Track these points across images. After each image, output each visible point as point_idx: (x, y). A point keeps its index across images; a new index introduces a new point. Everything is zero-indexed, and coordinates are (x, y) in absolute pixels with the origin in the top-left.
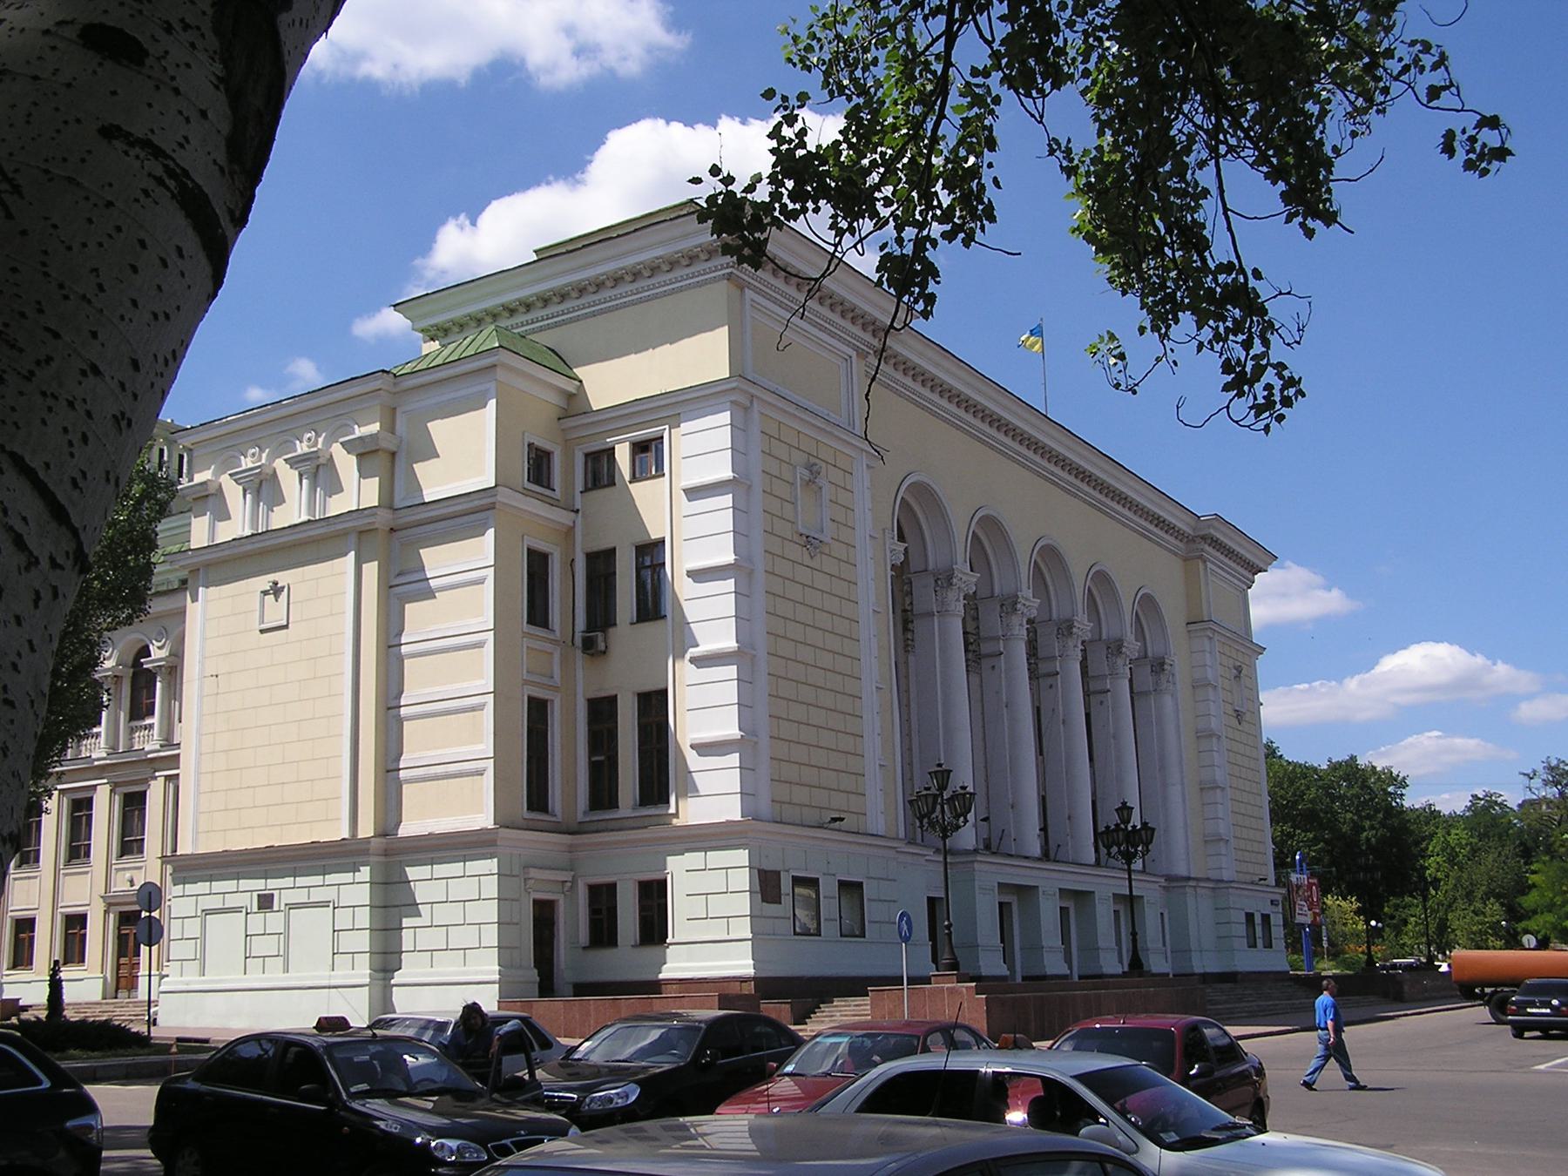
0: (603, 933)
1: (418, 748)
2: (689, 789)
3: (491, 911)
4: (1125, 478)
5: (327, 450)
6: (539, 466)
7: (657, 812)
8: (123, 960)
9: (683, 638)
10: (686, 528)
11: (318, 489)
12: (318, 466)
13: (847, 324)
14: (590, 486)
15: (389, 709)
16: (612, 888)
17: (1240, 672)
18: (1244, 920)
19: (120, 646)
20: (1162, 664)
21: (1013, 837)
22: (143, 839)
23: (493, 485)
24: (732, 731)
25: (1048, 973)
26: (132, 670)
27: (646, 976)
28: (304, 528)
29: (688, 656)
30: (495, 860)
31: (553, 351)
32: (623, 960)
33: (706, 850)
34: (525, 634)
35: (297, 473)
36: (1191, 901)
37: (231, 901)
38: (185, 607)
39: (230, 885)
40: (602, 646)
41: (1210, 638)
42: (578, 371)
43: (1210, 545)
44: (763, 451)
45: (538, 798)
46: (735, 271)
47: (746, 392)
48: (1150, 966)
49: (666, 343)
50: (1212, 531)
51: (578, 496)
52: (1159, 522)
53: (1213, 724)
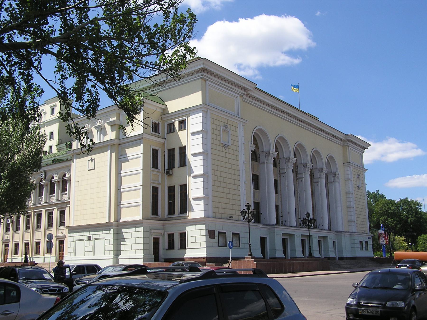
0: (171, 246)
1: (125, 199)
2: (192, 210)
3: (141, 240)
4: (323, 125)
5: (91, 128)
6: (155, 128)
7: (184, 215)
8: (60, 252)
9: (191, 171)
10: (191, 143)
11: (102, 134)
12: (102, 129)
13: (236, 89)
14: (169, 132)
15: (118, 189)
16: (173, 234)
17: (359, 176)
18: (359, 243)
19: (59, 174)
20: (336, 174)
21: (288, 221)
22: (64, 222)
23: (142, 133)
24: (202, 195)
25: (277, 257)
26: (62, 180)
27: (181, 257)
28: (76, 150)
29: (191, 176)
30: (143, 227)
31: (160, 98)
32: (175, 253)
33: (195, 225)
34: (151, 171)
35: (97, 130)
36: (343, 238)
37: (82, 238)
38: (71, 164)
39: (81, 234)
40: (171, 173)
41: (350, 167)
42: (166, 103)
43: (350, 142)
44: (211, 123)
45: (155, 211)
46: (203, 77)
47: (206, 108)
48: (314, 255)
49: (186, 95)
50: (350, 138)
51: (166, 135)
52: (334, 136)
53: (351, 190)
